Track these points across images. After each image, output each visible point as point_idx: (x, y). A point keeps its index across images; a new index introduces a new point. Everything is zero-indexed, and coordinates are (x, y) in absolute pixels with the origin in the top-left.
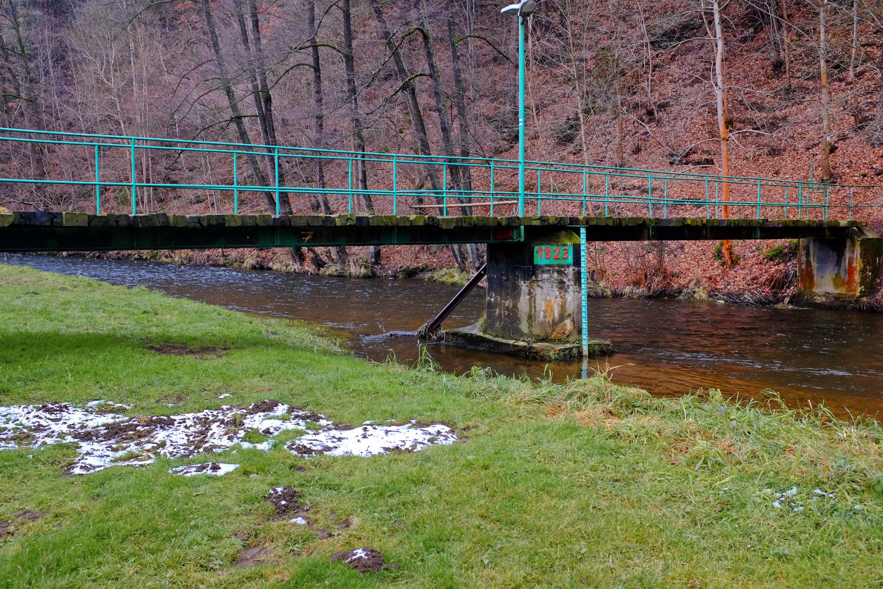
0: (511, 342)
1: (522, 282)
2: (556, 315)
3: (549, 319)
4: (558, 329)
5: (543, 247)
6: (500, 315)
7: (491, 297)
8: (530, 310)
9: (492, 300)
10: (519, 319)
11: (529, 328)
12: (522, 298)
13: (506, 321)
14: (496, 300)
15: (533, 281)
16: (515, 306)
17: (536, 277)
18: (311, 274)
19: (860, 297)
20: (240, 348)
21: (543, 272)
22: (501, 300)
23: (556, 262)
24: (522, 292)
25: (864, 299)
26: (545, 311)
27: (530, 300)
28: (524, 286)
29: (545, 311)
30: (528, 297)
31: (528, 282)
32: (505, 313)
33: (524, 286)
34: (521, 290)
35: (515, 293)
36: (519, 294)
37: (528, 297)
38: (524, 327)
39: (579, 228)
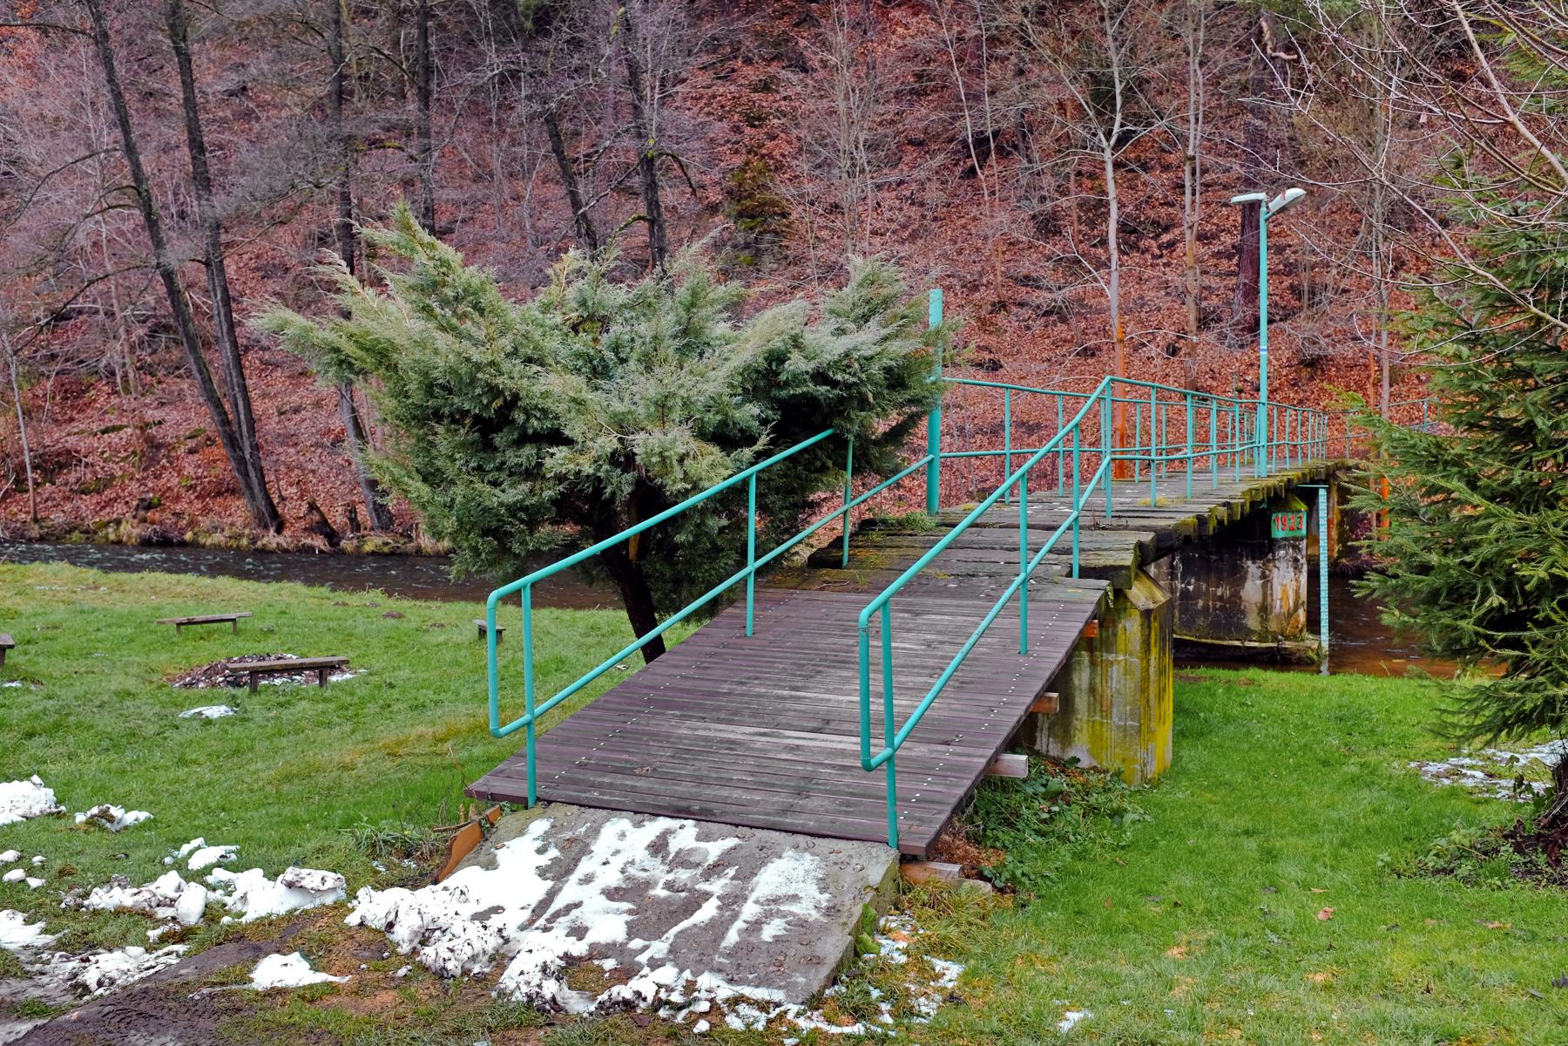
0: (1237, 643)
1: (1249, 563)
2: (1291, 604)
3: (1285, 610)
4: (1292, 621)
5: (1280, 515)
6: (1206, 608)
7: (1189, 584)
8: (1265, 598)
9: (1191, 588)
10: (1243, 613)
11: (1261, 623)
12: (1249, 585)
13: (1217, 616)
14: (1197, 588)
15: (1269, 561)
16: (1236, 596)
17: (1274, 555)
18: (321, 552)
19: (1339, 558)
20: (756, 1002)
21: (1280, 548)
22: (1207, 588)
23: (1291, 534)
24: (1250, 576)
25: (1344, 560)
26: (1281, 599)
27: (1264, 586)
28: (1253, 568)
29: (1281, 599)
30: (1259, 582)
31: (1260, 563)
32: (1214, 606)
33: (1253, 568)
34: (1247, 572)
35: (1238, 578)
36: (1244, 579)
37: (1259, 582)
38: (1252, 622)
39: (1317, 489)
